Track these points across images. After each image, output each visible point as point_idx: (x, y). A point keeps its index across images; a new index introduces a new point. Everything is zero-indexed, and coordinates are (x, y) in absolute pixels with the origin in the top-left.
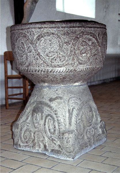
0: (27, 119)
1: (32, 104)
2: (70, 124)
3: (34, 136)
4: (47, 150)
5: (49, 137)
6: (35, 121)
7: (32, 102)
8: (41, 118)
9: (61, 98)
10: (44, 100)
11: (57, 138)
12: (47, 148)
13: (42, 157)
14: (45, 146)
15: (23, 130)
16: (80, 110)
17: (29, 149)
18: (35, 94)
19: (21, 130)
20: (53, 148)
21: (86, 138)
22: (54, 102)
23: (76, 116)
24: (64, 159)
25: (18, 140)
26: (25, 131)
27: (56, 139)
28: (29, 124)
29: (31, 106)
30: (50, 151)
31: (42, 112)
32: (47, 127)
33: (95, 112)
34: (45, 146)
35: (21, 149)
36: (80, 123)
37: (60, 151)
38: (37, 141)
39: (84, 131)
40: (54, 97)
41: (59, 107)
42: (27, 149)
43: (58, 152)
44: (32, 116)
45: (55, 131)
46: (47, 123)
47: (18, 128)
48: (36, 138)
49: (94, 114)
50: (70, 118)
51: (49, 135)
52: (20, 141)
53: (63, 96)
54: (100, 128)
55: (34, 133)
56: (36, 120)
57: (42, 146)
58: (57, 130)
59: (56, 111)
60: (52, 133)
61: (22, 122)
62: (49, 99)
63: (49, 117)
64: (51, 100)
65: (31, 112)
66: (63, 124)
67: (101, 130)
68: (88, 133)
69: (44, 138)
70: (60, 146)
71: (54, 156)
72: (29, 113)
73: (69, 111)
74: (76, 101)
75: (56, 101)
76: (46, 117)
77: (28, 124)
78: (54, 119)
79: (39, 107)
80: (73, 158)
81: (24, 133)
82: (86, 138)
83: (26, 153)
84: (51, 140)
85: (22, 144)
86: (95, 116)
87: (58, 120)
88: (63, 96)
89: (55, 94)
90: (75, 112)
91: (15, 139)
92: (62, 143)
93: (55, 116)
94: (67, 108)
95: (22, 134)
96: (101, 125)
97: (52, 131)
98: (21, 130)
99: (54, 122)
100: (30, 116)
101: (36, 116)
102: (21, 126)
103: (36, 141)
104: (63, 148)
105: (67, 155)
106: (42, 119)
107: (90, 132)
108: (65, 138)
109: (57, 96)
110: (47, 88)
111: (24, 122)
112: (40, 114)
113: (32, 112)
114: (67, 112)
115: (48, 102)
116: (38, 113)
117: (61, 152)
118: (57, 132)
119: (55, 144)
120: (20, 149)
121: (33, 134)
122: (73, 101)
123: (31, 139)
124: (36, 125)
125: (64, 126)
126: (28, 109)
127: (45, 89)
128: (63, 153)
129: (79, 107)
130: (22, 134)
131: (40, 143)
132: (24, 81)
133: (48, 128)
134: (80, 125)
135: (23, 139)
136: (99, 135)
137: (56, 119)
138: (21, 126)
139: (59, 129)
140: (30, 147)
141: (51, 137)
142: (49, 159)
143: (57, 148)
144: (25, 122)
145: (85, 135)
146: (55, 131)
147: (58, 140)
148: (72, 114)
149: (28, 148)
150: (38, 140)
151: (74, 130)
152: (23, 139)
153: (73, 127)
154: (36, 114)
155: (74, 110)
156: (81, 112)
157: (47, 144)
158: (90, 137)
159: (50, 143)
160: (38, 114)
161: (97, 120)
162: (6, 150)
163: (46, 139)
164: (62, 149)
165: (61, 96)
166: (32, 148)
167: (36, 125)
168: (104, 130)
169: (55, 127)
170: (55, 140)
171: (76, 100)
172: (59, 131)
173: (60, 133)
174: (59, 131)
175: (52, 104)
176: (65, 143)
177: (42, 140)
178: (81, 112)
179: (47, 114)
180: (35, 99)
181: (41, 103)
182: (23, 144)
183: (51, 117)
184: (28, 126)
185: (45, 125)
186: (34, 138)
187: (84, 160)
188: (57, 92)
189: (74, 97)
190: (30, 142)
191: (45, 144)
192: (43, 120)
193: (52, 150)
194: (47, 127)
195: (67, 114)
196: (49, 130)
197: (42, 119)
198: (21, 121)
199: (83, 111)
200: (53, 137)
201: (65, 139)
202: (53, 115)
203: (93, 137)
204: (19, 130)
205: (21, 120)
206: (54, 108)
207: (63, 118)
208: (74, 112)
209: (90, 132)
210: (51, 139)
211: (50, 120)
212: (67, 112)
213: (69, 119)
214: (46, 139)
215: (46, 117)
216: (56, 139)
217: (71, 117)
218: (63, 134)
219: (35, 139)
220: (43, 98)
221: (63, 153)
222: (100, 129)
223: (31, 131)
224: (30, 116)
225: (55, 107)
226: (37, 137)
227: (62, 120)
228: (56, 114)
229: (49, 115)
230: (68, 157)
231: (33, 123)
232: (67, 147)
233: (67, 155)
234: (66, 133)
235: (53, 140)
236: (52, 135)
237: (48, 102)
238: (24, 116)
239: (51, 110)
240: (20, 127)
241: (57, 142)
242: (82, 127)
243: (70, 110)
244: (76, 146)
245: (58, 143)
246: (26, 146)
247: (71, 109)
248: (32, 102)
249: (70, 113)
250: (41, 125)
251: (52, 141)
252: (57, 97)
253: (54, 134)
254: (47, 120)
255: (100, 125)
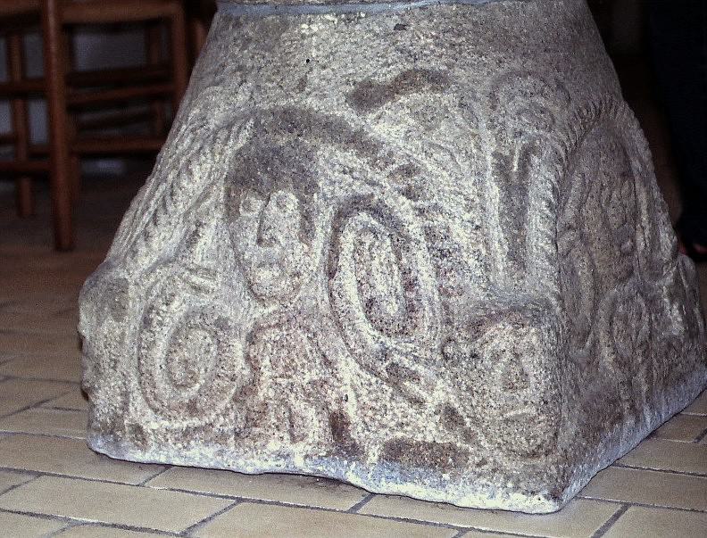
0: (192, 239)
1: (222, 135)
2: (517, 256)
3: (247, 358)
4: (354, 452)
5: (369, 360)
6: (253, 253)
7: (213, 124)
8: (303, 225)
9: (437, 80)
10: (312, 102)
11: (428, 362)
12: (356, 433)
13: (314, 497)
14: (338, 425)
15: (161, 324)
16: (567, 162)
17: (210, 451)
18: (231, 66)
19: (147, 322)
20: (399, 435)
21: (607, 357)
22: (387, 109)
23: (550, 205)
24: (491, 504)
25: (126, 395)
26: (178, 331)
27: (421, 369)
28: (210, 273)
29: (218, 146)
30: (374, 454)
31: (305, 185)
32: (351, 289)
33: (645, 183)
34: (338, 425)
35: (146, 457)
36: (575, 253)
37: (452, 447)
38: (271, 393)
39: (595, 308)
40: (385, 76)
41: (431, 145)
42: (201, 454)
43: (439, 459)
44: (231, 211)
45: (410, 309)
46: (345, 262)
47: (119, 312)
48: (267, 373)
49: (643, 197)
50: (516, 219)
51: (370, 342)
52: (137, 402)
53: (450, 66)
54: (672, 297)
55: (252, 339)
56: (260, 241)
57: (315, 426)
58: (425, 303)
59: (408, 171)
60: (394, 328)
61: (152, 270)
62: (350, 89)
63: (364, 216)
64: (366, 97)
65: (219, 193)
66: (472, 262)
67: (680, 308)
68: (618, 325)
69: (327, 363)
70: (451, 416)
71: (408, 489)
72: (206, 195)
73: (502, 168)
74: (541, 101)
75: (403, 99)
76: (342, 215)
77: (196, 279)
78: (395, 226)
79: (277, 151)
80: (555, 496)
81: (174, 343)
82: (607, 357)
83: (192, 483)
84: (385, 374)
85: (152, 423)
86: (644, 212)
87: (429, 233)
88: (450, 66)
89: (393, 55)
90: (542, 179)
91: (101, 394)
92: (469, 389)
93: (403, 208)
94: (490, 147)
95: (159, 353)
96: (677, 281)
97: (392, 309)
98: (147, 322)
99: (402, 243)
100: (215, 220)
101: (262, 217)
102: (148, 293)
103: (265, 392)
104: (478, 425)
105: (508, 478)
106: (306, 232)
107: (625, 320)
108: (496, 357)
109: (409, 67)
110: (328, 17)
111: (165, 262)
112: (292, 201)
113: (228, 192)
114: (488, 174)
115: (348, 115)
116: (274, 197)
117: (466, 453)
118: (426, 316)
119: (418, 402)
120: (138, 456)
121: (238, 346)
122: (521, 101)
123: (225, 383)
124: (265, 276)
125: (478, 273)
126: (196, 169)
127: (310, 22)
128: (483, 462)
129: (563, 145)
130: (159, 353)
131: (298, 405)
132: (16, 59)
133: (360, 291)
134: (573, 272)
135: (163, 387)
136: (670, 345)
137: (414, 227)
138: (148, 293)
139: (444, 292)
140: (222, 438)
141: (385, 354)
142: (371, 507)
143: (429, 430)
144: (175, 268)
145: (603, 341)
146: (410, 309)
147: (440, 375)
148: (523, 190)
149: (206, 443)
150: (284, 382)
151: (547, 301)
152: (163, 387)
153: (541, 279)
154: (257, 204)
155: (535, 160)
156: (577, 181)
157: (351, 410)
158: (629, 354)
159: (376, 400)
160: (272, 204)
161: (654, 241)
162: (39, 475)
163: (348, 369)
164: (468, 436)
165: (437, 65)
166: (238, 446)
167: (265, 276)
168: (697, 311)
169: (410, 285)
170: (414, 377)
171: (541, 93)
172: (446, 306)
173: (449, 322)
174: (446, 306)
175: (376, 128)
176: (497, 389)
177: (313, 383)
178: (577, 181)
179: (341, 194)
180: (241, 98)
181: (291, 120)
182: (166, 423)
183: (376, 211)
184: (197, 289)
185: (331, 274)
186: (247, 372)
187: (626, 506)
188: (404, 39)
189: (525, 74)
190: (221, 406)
191: (334, 407)
192: (319, 243)
193: (394, 451)
194: (351, 289)
195: (494, 191)
196: (370, 304)
197: (306, 232)
198: (145, 262)
199: (586, 170)
200: (397, 358)
201: (488, 363)
202: (389, 202)
203: (646, 354)
204: (132, 323)
205: (143, 249)
206: (391, 154)
207: (467, 216)
208: (532, 175)
209: (625, 320)
210: (382, 367)
211: (368, 239)
212: (488, 174)
213: (505, 226)
214: (348, 369)
215: (342, 215)
216: (421, 369)
217: (522, 211)
218: (476, 327)
219: (254, 382)
220: (303, 83)
221: (483, 462)
222: (672, 303)
223: (222, 324)
224: (214, 223)
225: (401, 144)
226: (274, 365)
227: (461, 235)
228: (408, 193)
229: (357, 203)
230: (516, 488)
231: (241, 264)
232: (507, 421)
233: (508, 478)
234: (492, 319)
235: (396, 376)
236: (391, 343)
237: (348, 115)
238: (162, 219)
239: (373, 164)
240: (135, 307)
241: (430, 387)
242: (586, 284)
243: (508, 161)
244: (565, 415)
245: (441, 393)
246: (187, 434)
247: (512, 153)
248: (213, 124)
249: (515, 187)
250: (298, 274)
251: (395, 385)
252: (404, 76)
253: (403, 332)
254: (348, 240)
255: (669, 280)
